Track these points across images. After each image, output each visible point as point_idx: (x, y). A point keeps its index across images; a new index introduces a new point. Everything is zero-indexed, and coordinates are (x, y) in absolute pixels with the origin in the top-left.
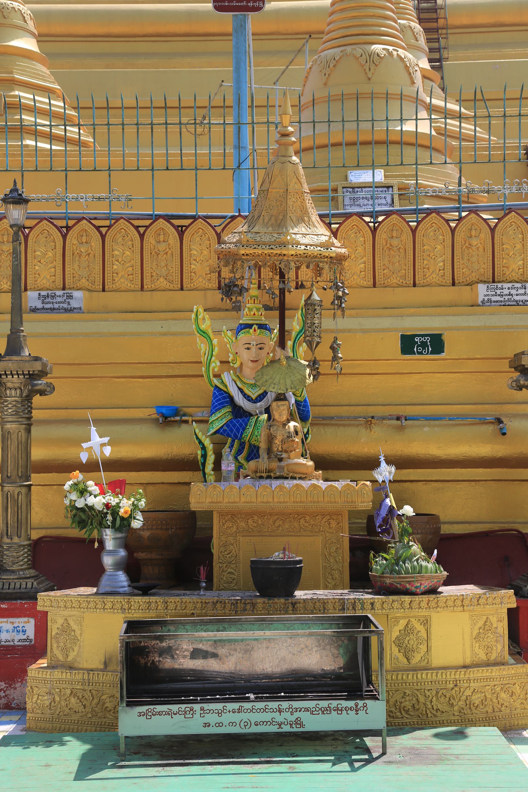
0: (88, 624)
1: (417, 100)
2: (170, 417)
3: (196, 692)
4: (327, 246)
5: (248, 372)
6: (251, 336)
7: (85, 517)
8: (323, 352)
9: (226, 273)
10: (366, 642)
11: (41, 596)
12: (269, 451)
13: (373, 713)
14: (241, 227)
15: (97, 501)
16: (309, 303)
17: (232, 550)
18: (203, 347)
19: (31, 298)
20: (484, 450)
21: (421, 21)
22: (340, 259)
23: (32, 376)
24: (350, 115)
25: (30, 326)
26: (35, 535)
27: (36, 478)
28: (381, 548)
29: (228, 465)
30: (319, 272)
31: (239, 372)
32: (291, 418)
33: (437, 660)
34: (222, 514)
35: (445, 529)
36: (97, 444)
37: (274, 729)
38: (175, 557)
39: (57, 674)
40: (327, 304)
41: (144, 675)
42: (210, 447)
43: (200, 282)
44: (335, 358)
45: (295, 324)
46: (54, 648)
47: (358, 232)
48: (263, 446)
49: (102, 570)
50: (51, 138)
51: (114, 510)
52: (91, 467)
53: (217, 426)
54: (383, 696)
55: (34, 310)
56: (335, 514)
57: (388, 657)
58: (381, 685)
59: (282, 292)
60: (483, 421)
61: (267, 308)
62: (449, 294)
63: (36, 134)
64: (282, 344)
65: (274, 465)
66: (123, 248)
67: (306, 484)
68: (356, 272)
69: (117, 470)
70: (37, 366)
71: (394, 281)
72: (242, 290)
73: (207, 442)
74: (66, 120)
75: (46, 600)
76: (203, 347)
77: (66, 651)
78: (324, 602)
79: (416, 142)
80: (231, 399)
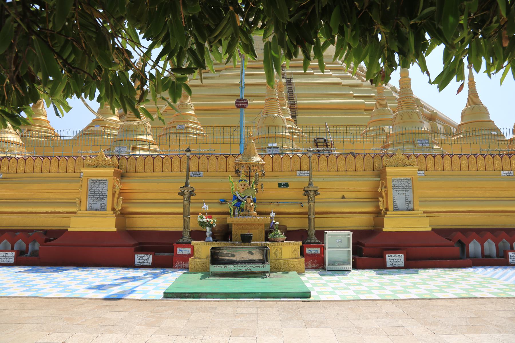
0: (203, 249)
1: (286, 127)
2: (223, 202)
3: (227, 263)
4: (260, 161)
5: (242, 191)
6: (243, 182)
7: (202, 224)
8: (259, 186)
9: (237, 168)
10: (267, 251)
11: (192, 242)
12: (246, 210)
13: (267, 267)
14: (240, 157)
15: (205, 220)
16: (256, 175)
17: (237, 232)
18: (231, 185)
19: (191, 173)
20: (298, 210)
21: (290, 109)
22: (263, 165)
23: (191, 191)
24: (267, 131)
25: (191, 180)
26: (191, 230)
27: (191, 216)
28: (271, 232)
29: (236, 213)
30: (259, 168)
31: (239, 191)
32: (252, 202)
33: (283, 258)
34: (234, 224)
35: (288, 229)
36: (205, 207)
37: (245, 271)
38: (224, 234)
39: (196, 260)
40: (260, 175)
41: (215, 258)
42: (232, 209)
43: (231, 170)
44: (262, 188)
45: (253, 180)
46: (195, 254)
47: (268, 158)
48: (245, 208)
49: (206, 236)
50: (197, 134)
51: (209, 222)
52: (204, 214)
53: (234, 204)
54: (269, 263)
55: (191, 176)
56: (261, 225)
57: (272, 256)
58: (269, 261)
59: (250, 172)
60: (298, 204)
61: (246, 176)
62: (290, 173)
63: (193, 134)
64: (250, 184)
65: (247, 213)
66: (213, 162)
67: (254, 217)
68: (268, 168)
69: (210, 214)
70: (192, 189)
71: (277, 170)
72: (240, 172)
73: (231, 208)
74: (200, 130)
75: (193, 243)
76: (231, 185)
77: (198, 255)
78: (257, 244)
79: (285, 137)
80: (237, 197)
